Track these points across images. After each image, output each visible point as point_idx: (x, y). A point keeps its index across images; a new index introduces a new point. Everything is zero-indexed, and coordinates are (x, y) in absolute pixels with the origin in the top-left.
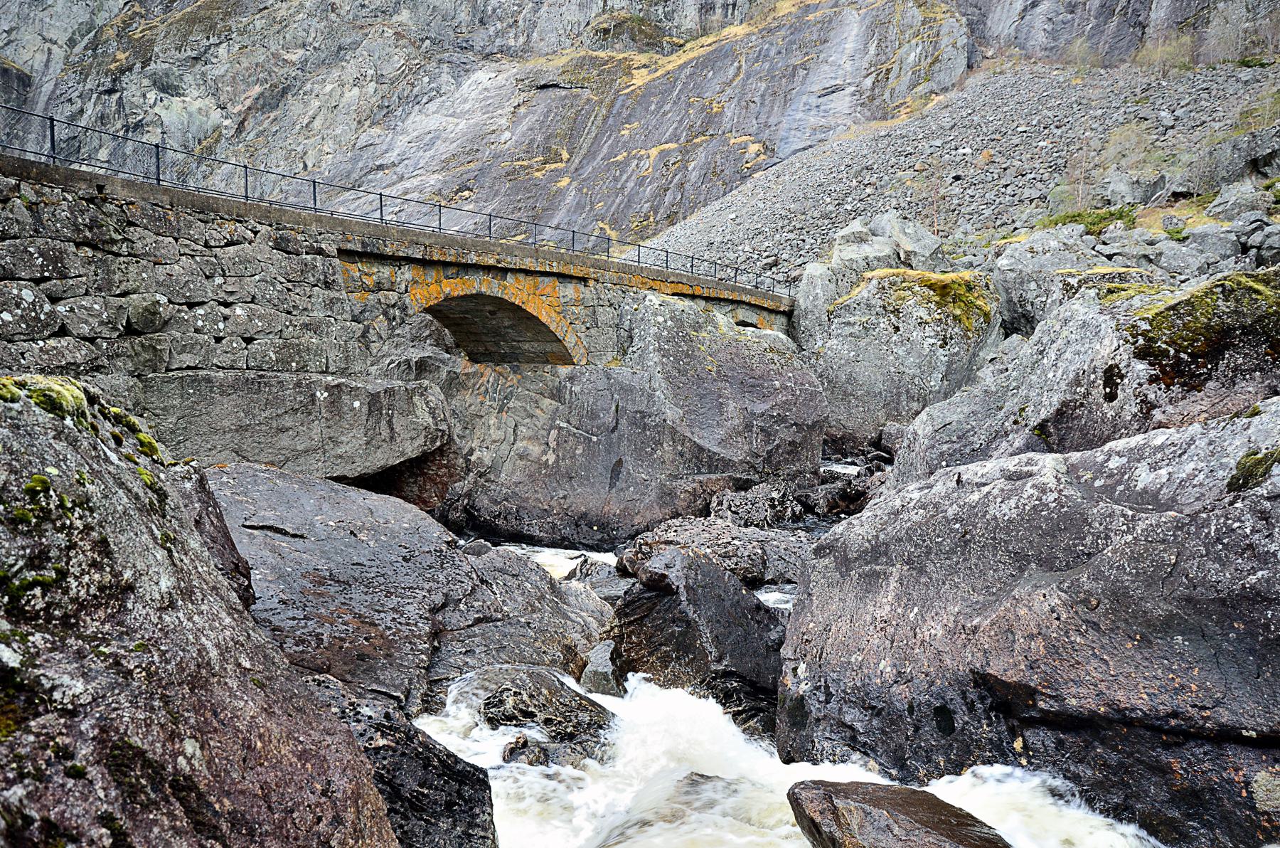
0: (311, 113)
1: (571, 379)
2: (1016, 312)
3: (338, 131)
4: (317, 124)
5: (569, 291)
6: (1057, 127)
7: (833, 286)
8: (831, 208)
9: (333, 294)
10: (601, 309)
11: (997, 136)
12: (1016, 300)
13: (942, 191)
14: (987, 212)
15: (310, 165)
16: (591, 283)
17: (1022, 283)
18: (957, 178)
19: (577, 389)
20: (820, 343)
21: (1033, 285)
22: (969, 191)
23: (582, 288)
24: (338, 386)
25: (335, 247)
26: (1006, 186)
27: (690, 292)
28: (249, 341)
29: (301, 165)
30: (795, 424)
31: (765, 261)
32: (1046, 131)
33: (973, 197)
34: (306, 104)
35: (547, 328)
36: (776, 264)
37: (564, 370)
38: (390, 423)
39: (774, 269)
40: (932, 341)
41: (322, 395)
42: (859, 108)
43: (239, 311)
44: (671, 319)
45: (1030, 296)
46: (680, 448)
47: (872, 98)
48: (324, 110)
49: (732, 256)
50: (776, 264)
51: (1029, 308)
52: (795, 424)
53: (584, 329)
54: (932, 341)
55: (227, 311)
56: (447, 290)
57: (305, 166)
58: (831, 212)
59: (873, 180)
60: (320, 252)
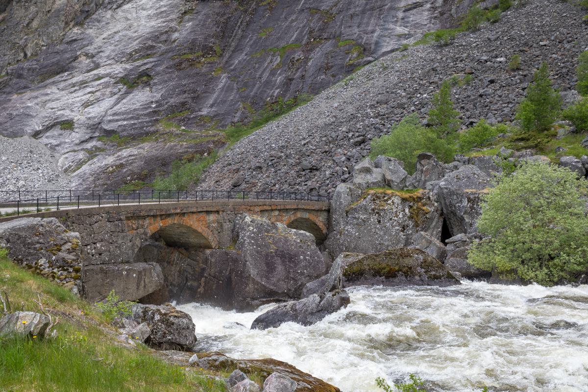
0: (30, 16)
1: (212, 255)
2: (448, 210)
3: (50, 30)
4: (35, 24)
5: (212, 217)
6: (568, 42)
7: (349, 198)
8: (404, 100)
9: (125, 234)
10: (224, 224)
11: (526, 49)
12: (448, 204)
13: (481, 91)
14: (506, 110)
15: (29, 54)
16: (221, 213)
17: (451, 195)
18: (492, 82)
19: (213, 260)
20: (342, 227)
21: (455, 197)
22: (499, 92)
23: (217, 215)
24: (129, 269)
25: (125, 216)
26: (524, 89)
27: (270, 208)
28: (100, 254)
29: (22, 55)
30: (308, 276)
31: (357, 139)
32: (560, 45)
33: (500, 96)
34: (27, 9)
35: (201, 234)
36: (363, 142)
37: (208, 251)
38: (144, 281)
39: (362, 146)
40: (397, 228)
41: (125, 273)
42: (433, 21)
43: (98, 245)
44: (256, 228)
45: (454, 202)
46: (256, 287)
47: (442, 14)
48: (40, 14)
49: (334, 135)
50: (363, 142)
51: (454, 208)
52: (308, 276)
53: (217, 232)
54: (397, 228)
55: (95, 246)
56: (161, 224)
57: (26, 55)
58: (405, 104)
59: (436, 79)
60: (120, 220)
